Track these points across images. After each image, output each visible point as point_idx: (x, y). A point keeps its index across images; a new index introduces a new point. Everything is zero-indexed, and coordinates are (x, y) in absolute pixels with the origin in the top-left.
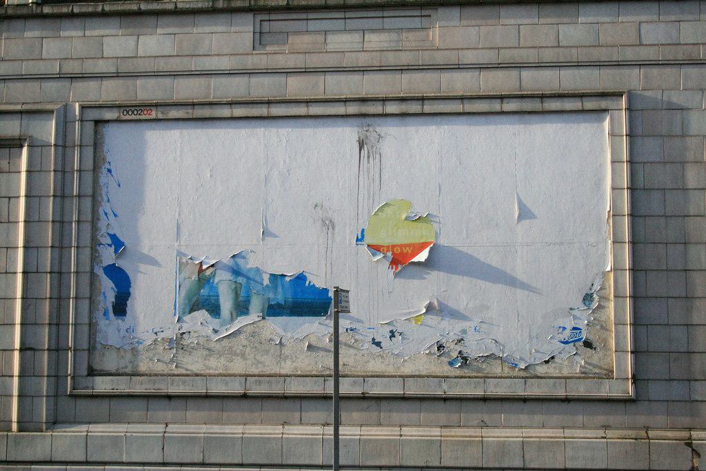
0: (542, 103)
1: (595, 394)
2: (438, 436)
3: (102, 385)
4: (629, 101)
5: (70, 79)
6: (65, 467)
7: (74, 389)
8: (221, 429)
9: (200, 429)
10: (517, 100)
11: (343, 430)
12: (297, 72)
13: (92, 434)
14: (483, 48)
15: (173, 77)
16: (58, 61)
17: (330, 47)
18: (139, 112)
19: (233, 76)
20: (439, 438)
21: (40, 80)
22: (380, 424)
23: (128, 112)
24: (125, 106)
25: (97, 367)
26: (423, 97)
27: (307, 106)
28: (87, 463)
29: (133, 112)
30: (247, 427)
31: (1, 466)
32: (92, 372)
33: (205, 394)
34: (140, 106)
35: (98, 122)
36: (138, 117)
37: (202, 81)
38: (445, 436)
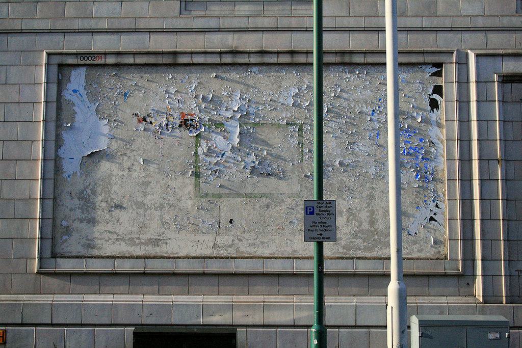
0: (307, 57)
1: (226, 270)
2: (230, 302)
3: (66, 265)
4: (458, 57)
5: (436, 32)
6: (275, 329)
7: (40, 268)
8: (17, 297)
9: (169, 299)
10: (203, 55)
11: (327, 299)
12: (332, 30)
13: (145, 303)
14: (487, 16)
15: (91, 34)
16: (379, 15)
17: (237, 13)
18: (93, 58)
19: (82, 34)
20: (293, 303)
21: (120, 33)
22: (188, 294)
23: (84, 58)
24: (81, 54)
25: (59, 250)
26: (307, 50)
27: (423, 56)
28: (52, 325)
29: (88, 58)
30: (55, 296)
31: (1, 328)
32: (54, 256)
33: (203, 272)
34: (86, 54)
35: (60, 66)
36: (92, 62)
37: (288, 35)
38: (235, 302)
